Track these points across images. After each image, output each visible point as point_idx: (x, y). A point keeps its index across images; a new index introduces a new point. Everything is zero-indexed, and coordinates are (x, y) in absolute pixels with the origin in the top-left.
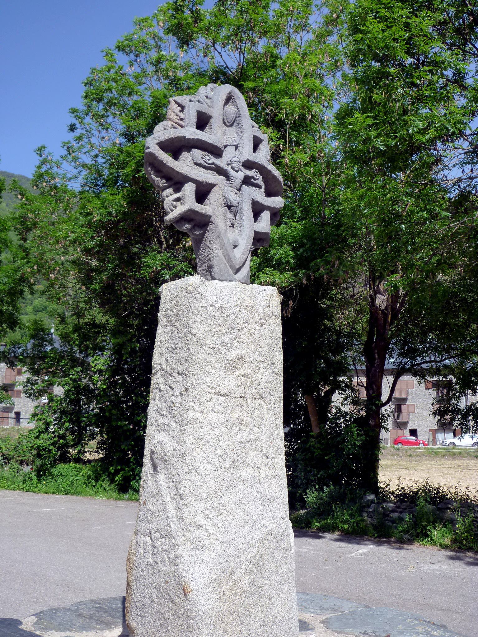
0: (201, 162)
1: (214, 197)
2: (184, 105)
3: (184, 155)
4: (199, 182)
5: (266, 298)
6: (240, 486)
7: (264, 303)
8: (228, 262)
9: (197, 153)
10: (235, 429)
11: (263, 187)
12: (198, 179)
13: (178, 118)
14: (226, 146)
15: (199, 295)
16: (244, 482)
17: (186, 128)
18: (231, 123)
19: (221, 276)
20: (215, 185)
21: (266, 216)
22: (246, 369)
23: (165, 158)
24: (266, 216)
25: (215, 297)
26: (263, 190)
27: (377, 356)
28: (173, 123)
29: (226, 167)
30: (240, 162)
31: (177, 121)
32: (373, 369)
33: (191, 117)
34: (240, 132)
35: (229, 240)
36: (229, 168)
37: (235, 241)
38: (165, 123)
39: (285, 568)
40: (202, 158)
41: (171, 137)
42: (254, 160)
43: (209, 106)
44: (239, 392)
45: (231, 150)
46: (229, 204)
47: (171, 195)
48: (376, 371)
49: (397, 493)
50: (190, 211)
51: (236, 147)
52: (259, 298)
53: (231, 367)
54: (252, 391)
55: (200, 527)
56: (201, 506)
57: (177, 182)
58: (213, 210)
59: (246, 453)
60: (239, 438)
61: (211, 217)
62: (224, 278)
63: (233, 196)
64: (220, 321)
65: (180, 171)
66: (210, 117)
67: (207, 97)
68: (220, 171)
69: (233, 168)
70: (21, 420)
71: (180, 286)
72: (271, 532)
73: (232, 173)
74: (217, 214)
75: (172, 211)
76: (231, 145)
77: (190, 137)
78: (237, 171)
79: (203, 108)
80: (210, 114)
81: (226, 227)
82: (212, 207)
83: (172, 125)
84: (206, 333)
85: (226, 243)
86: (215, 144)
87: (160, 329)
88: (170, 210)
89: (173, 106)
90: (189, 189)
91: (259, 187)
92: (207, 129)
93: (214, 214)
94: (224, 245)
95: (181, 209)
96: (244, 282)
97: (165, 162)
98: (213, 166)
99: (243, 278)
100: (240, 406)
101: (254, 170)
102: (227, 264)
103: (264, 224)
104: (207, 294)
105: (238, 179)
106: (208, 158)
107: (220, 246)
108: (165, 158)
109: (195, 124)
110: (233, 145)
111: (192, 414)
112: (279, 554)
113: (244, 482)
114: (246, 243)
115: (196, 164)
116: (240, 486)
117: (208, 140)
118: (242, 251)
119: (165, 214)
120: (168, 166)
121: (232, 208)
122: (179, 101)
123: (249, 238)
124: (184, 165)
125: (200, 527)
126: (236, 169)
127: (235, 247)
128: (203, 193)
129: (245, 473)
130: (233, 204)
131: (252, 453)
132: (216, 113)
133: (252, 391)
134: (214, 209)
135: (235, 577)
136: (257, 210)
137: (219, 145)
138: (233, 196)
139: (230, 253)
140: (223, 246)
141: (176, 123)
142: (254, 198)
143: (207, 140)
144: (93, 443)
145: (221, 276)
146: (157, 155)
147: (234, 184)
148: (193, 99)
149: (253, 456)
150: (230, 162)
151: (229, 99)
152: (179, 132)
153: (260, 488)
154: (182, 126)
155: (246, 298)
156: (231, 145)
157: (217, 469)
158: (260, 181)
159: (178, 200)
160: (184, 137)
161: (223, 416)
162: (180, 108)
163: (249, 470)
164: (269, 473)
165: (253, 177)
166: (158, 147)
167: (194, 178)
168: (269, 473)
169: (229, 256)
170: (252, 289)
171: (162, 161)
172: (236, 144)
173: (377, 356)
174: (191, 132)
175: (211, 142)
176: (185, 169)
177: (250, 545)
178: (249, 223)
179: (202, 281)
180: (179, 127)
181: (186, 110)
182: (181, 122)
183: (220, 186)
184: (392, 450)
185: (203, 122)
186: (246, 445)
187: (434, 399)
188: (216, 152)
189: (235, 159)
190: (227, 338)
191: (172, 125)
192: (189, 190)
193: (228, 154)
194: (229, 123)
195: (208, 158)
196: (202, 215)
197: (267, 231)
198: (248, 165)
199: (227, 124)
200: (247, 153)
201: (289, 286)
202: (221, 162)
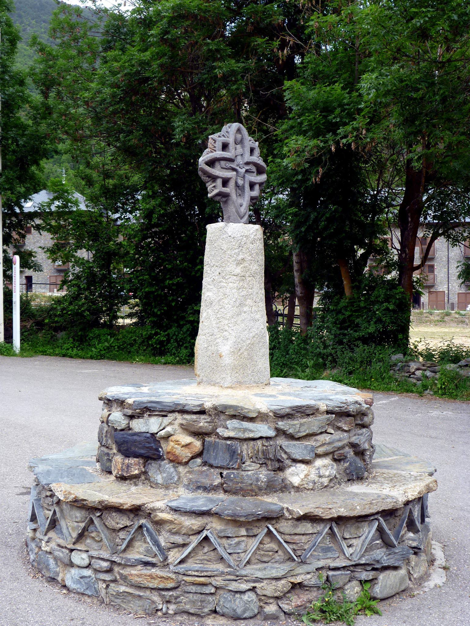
1: (232, 184)
3: (217, 164)
6: (243, 314)
9: (223, 163)
10: (241, 290)
16: (245, 312)
21: (257, 187)
22: (246, 264)
23: (207, 168)
24: (257, 187)
26: (255, 174)
27: (410, 220)
32: (406, 232)
33: (219, 145)
36: (238, 168)
38: (207, 150)
39: (264, 350)
44: (242, 274)
48: (409, 234)
49: (424, 353)
50: (220, 192)
52: (251, 231)
53: (238, 264)
54: (248, 273)
55: (226, 331)
56: (226, 322)
57: (214, 178)
59: (246, 300)
60: (242, 294)
64: (234, 244)
68: (234, 170)
70: (33, 286)
72: (257, 334)
73: (240, 170)
82: (230, 189)
84: (228, 249)
87: (207, 246)
89: (210, 140)
90: (219, 182)
91: (253, 172)
95: (216, 191)
100: (243, 280)
103: (256, 193)
108: (207, 168)
111: (222, 284)
112: (261, 344)
113: (245, 312)
116: (243, 314)
118: (244, 209)
124: (216, 171)
125: (226, 331)
127: (241, 206)
128: (225, 182)
129: (245, 309)
131: (248, 300)
132: (231, 140)
133: (248, 273)
135: (241, 351)
136: (252, 186)
140: (235, 206)
144: (125, 309)
149: (249, 302)
151: (239, 131)
153: (252, 315)
157: (233, 307)
158: (254, 169)
159: (214, 187)
161: (235, 285)
163: (247, 307)
164: (256, 309)
168: (256, 309)
173: (410, 220)
174: (219, 154)
177: (247, 339)
184: (457, 316)
185: (225, 147)
186: (245, 297)
187: (458, 262)
188: (231, 160)
190: (237, 251)
193: (239, 160)
198: (247, 163)
200: (248, 158)
201: (317, 153)
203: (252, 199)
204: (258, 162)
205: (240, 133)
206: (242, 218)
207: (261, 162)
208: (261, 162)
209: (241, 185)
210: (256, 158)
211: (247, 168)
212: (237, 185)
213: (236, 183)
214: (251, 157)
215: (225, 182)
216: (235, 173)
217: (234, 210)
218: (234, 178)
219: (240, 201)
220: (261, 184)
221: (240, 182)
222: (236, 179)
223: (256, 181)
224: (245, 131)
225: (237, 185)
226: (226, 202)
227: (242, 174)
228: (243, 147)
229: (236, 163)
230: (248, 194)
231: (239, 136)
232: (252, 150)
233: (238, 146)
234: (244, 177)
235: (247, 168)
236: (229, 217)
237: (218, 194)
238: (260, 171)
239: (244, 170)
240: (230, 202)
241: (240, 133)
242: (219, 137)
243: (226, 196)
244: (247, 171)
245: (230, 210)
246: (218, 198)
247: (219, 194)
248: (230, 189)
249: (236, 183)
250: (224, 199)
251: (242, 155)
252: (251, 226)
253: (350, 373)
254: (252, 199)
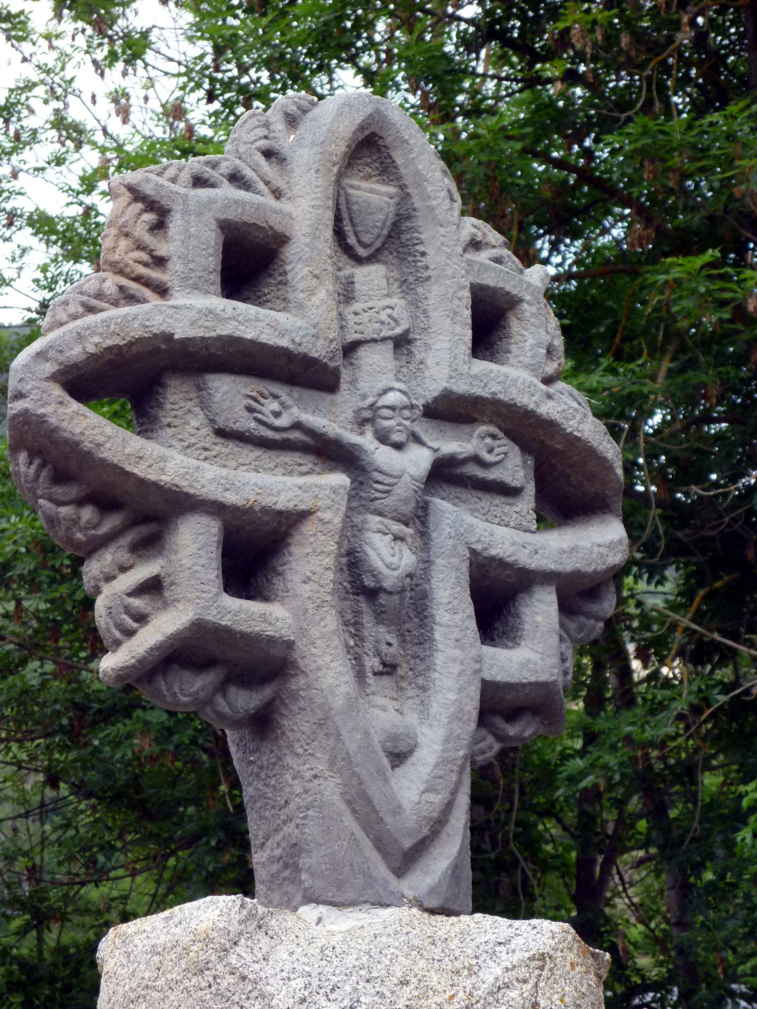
0: (247, 424)
2: (165, 202)
3: (177, 397)
4: (234, 509)
5: (522, 973)
7: (513, 994)
8: (367, 828)
9: (229, 393)
11: (530, 490)
12: (231, 498)
13: (145, 257)
14: (350, 349)
15: (231, 979)
17: (179, 299)
18: (371, 242)
19: (340, 887)
20: (303, 515)
21: (541, 611)
23: (91, 427)
24: (541, 611)
25: (298, 983)
26: (526, 504)
28: (124, 282)
29: (352, 437)
30: (412, 407)
31: (142, 270)
34: (410, 284)
35: (367, 734)
36: (366, 441)
37: (394, 738)
40: (250, 410)
41: (109, 342)
42: (477, 391)
43: (277, 194)
45: (377, 358)
46: (369, 582)
47: (123, 569)
50: (199, 628)
51: (402, 343)
52: (491, 973)
57: (149, 514)
58: (295, 615)
61: (290, 645)
62: (350, 895)
63: (385, 552)
65: (152, 477)
66: (282, 240)
67: (268, 154)
68: (330, 452)
69: (383, 438)
71: (163, 939)
73: (382, 456)
74: (315, 632)
75: (130, 633)
76: (375, 341)
77: (191, 333)
78: (398, 447)
79: (250, 205)
80: (279, 228)
81: (360, 676)
82: (300, 609)
83: (121, 288)
85: (352, 748)
86: (301, 349)
88: (117, 634)
90: (194, 546)
92: (268, 289)
93: (303, 632)
94: (348, 758)
95: (164, 626)
96: (434, 903)
97: (87, 445)
98: (296, 435)
99: (432, 891)
101: (483, 428)
102: (360, 834)
103: (536, 652)
104: (268, 971)
105: (406, 479)
106: (275, 406)
107: (332, 763)
108: (91, 427)
109: (216, 278)
110: (384, 339)
114: (447, 741)
115: (223, 434)
117: (269, 338)
119: (98, 647)
120: (103, 461)
121: (383, 599)
122: (148, 190)
123: (456, 717)
124: (170, 456)
126: (396, 437)
127: (399, 757)
128: (252, 553)
130: (387, 584)
132: (301, 212)
134: (301, 614)
136: (496, 599)
137: (318, 350)
138: (385, 552)
139: (374, 791)
140: (342, 762)
141: (137, 279)
142: (478, 547)
143: (263, 339)
145: (340, 887)
146: (53, 421)
147: (390, 501)
148: (208, 172)
150: (367, 414)
152: (150, 317)
154: (162, 291)
155: (434, 979)
156: (375, 341)
158: (514, 468)
159: (153, 587)
160: (168, 338)
162: (150, 217)
165: (476, 460)
166: (57, 391)
167: (212, 497)
169: (369, 801)
170: (463, 934)
171: (77, 444)
172: (398, 331)
175: (284, 343)
176: (171, 467)
178: (457, 653)
179: (252, 916)
180: (147, 293)
181: (175, 224)
182: (155, 274)
183: (327, 515)
188: (312, 375)
189: (392, 398)
191: (121, 288)
192: (192, 548)
193: (374, 375)
194: (365, 246)
195: (275, 406)
196: (252, 641)
197: (544, 677)
198: (451, 410)
199: (362, 252)
200: (446, 361)
202: (330, 418)
203: (498, 704)
204: (548, 409)
205: (387, 170)
206: (405, 860)
207: (570, 410)
208: (570, 410)
209: (390, 579)
210: (529, 371)
211: (454, 444)
212: (358, 582)
213: (353, 564)
214: (481, 366)
215: (252, 553)
216: (340, 479)
217: (331, 789)
218: (333, 516)
219: (384, 713)
220: (576, 593)
221: (388, 555)
222: (351, 530)
223: (533, 563)
224: (420, 153)
225: (358, 582)
226: (263, 724)
227: (404, 491)
228: (410, 284)
229: (347, 401)
230: (458, 660)
231: (373, 195)
232: (489, 322)
233: (371, 278)
234: (419, 518)
235: (454, 444)
236: (291, 860)
237: (180, 655)
238: (564, 496)
239: (417, 461)
240: (297, 724)
241: (387, 170)
242: (199, 181)
243: (266, 666)
244: (445, 474)
245: (297, 793)
246: (187, 688)
247: (192, 651)
248: (300, 609)
249: (353, 564)
250: (245, 700)
251: (402, 343)
252: (490, 927)
253: (295, 845)
254: (498, 704)
